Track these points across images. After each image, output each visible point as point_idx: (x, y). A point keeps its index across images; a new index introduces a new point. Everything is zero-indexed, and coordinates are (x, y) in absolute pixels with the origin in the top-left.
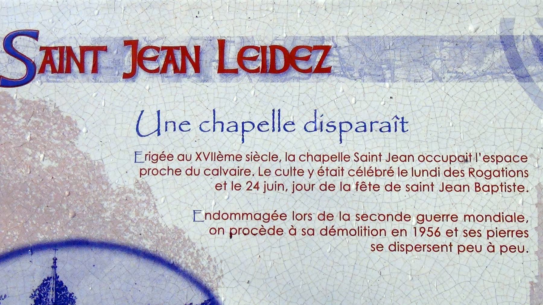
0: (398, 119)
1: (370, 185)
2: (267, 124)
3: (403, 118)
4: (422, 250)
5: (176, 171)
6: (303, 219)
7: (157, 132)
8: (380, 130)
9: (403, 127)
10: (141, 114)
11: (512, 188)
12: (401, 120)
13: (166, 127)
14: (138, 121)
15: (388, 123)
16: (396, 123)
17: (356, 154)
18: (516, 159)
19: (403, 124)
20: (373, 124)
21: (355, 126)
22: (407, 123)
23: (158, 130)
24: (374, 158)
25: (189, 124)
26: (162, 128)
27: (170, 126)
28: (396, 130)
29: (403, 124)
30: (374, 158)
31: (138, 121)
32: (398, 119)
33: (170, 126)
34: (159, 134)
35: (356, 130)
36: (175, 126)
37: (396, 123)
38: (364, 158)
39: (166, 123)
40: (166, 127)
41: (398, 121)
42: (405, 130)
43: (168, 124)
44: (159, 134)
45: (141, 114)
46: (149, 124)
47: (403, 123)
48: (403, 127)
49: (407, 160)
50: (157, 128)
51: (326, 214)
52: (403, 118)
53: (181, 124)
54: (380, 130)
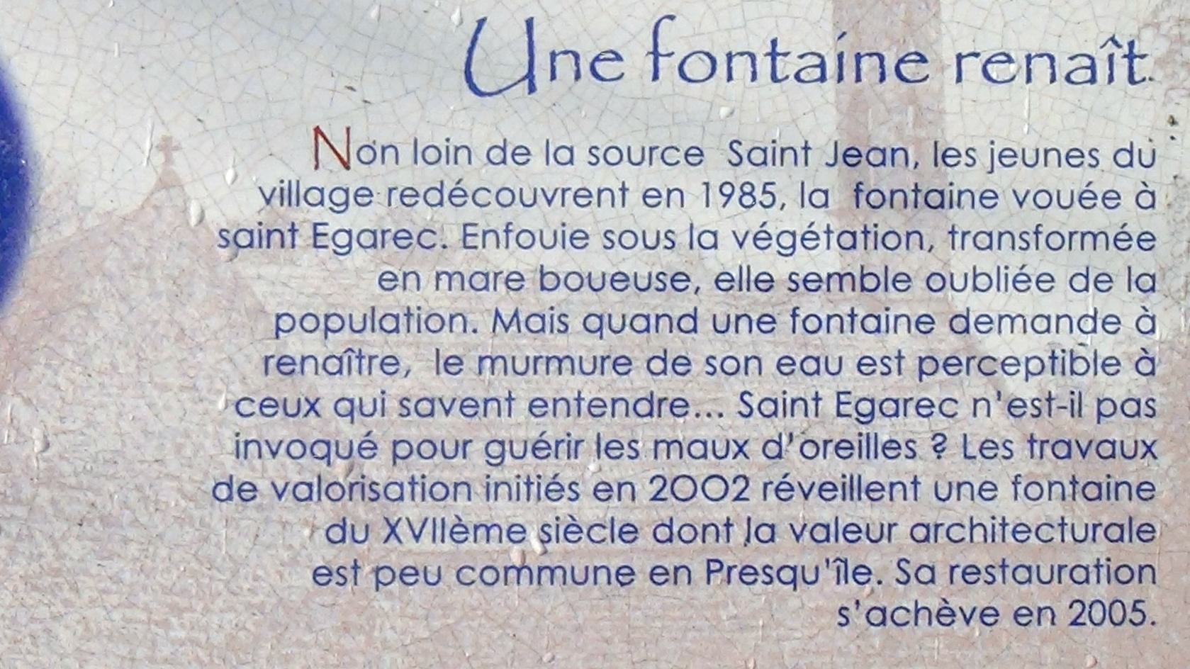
0: (1119, 46)
1: (828, 232)
2: (1010, 60)
3: (1131, 44)
4: (551, 413)
5: (982, 197)
6: (446, 328)
7: (527, 81)
8: (797, 77)
9: (1131, 68)
10: (478, 30)
11: (1031, 238)
12: (1126, 50)
13: (1029, 71)
14: (470, 51)
15: (819, 56)
16: (1111, 57)
17: (735, 146)
18: (671, 156)
19: (774, 60)
20: (964, 61)
21: (1063, 66)
22: (786, 54)
23: (530, 76)
24: (789, 155)
25: (619, 58)
26: (542, 75)
27: (565, 66)
28: (1111, 79)
29: (774, 60)
30: (789, 155)
31: (470, 51)
32: (1119, 46)
33: (565, 66)
34: (532, 89)
35: (1068, 79)
36: (577, 64)
37: (1111, 57)
38: (757, 156)
39: (553, 55)
40: (1029, 71)
41: (1118, 53)
42: (779, 76)
43: (735, 60)
44: (532, 89)
45: (478, 30)
46: (502, 58)
47: (1130, 57)
48: (1131, 68)
49: (888, 162)
50: (525, 71)
51: (1100, 317)
52: (1131, 44)
53: (597, 59)
54: (797, 77)
